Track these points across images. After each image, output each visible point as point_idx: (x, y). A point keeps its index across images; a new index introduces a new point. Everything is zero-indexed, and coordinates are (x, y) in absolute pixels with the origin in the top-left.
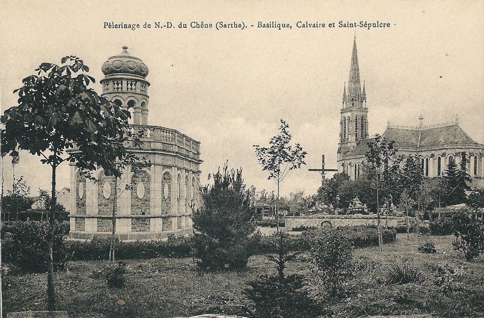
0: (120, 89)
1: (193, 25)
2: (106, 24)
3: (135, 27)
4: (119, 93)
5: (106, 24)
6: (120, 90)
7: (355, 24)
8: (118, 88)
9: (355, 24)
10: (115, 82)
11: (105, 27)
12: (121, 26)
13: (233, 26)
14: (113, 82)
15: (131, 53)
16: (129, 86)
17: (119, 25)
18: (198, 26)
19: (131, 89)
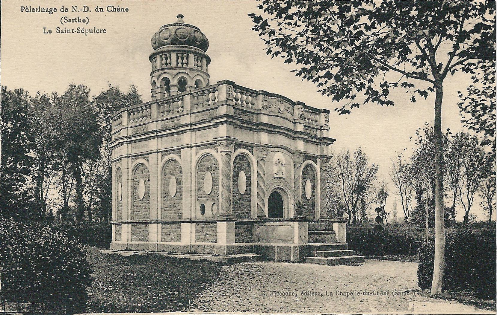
0: (169, 64)
1: (110, 9)
2: (22, 8)
3: (53, 11)
4: (168, 69)
5: (22, 8)
6: (169, 66)
7: (73, 30)
8: (166, 64)
9: (73, 30)
10: (163, 56)
11: (22, 11)
12: (38, 10)
13: (77, 20)
14: (161, 56)
15: (186, 21)
16: (180, 60)
17: (37, 9)
18: (114, 10)
19: (166, 64)
